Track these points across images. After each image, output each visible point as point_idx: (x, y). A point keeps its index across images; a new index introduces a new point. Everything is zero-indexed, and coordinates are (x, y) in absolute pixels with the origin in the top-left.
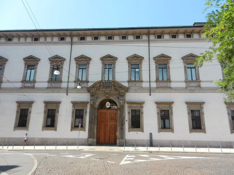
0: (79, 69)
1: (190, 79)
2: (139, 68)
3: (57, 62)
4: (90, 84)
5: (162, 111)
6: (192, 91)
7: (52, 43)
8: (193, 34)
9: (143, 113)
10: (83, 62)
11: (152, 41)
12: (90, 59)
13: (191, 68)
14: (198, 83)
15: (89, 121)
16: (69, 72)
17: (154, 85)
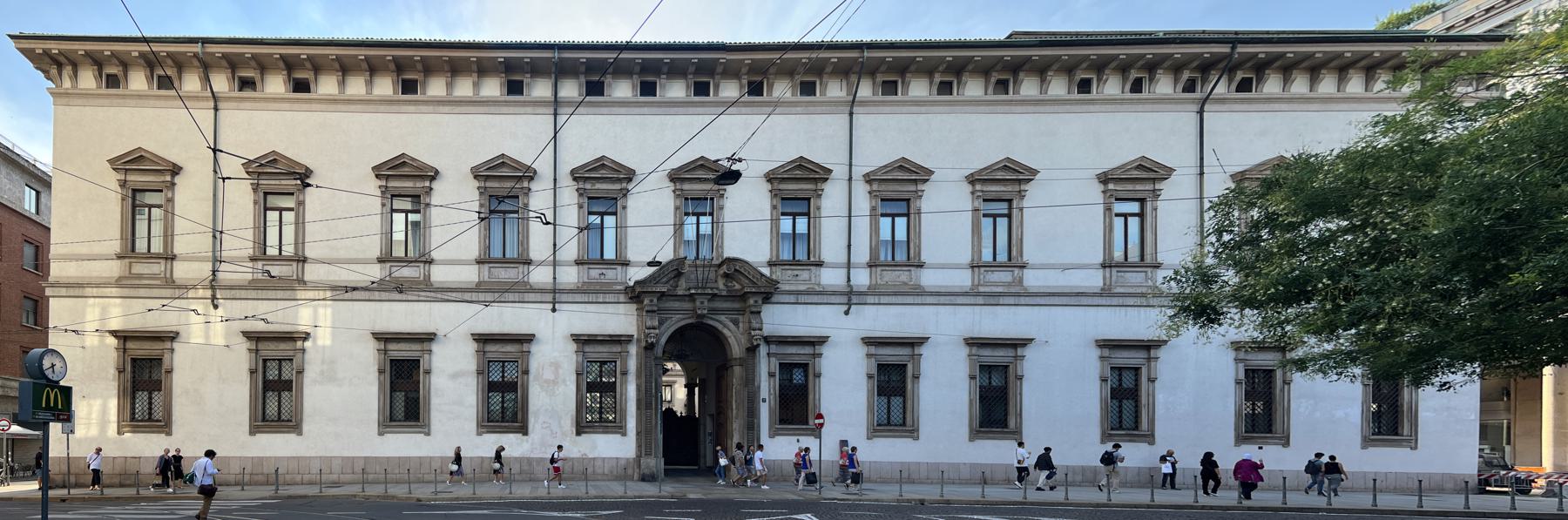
0: (393, 211)
1: (987, 256)
2: (615, 214)
3: (405, 181)
4: (637, 274)
5: (882, 368)
6: (993, 298)
7: (367, 102)
8: (1021, 75)
9: (1020, 378)
10: (604, 186)
11: (864, 103)
12: (629, 175)
13: (995, 216)
14: (1016, 271)
15: (639, 401)
16: (553, 229)
17: (570, 276)
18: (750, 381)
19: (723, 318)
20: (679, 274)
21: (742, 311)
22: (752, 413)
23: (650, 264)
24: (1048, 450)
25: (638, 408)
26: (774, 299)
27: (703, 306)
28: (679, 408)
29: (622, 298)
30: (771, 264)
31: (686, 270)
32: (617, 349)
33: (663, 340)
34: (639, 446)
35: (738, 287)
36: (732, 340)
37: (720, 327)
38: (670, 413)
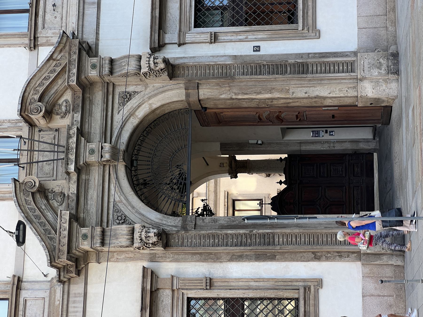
15: (260, 257)
18: (224, 72)
19: (118, 118)
20: (43, 191)
21: (109, 88)
22: (279, 67)
23: (21, 240)
24: (277, 183)
25: (272, 257)
26: (90, 38)
27: (96, 151)
28: (272, 186)
29: (77, 288)
30: (34, 44)
31: (35, 179)
32: (165, 297)
33: (154, 216)
34: (340, 256)
35: (68, 96)
36: (156, 102)
37: (133, 122)
38: (281, 203)
